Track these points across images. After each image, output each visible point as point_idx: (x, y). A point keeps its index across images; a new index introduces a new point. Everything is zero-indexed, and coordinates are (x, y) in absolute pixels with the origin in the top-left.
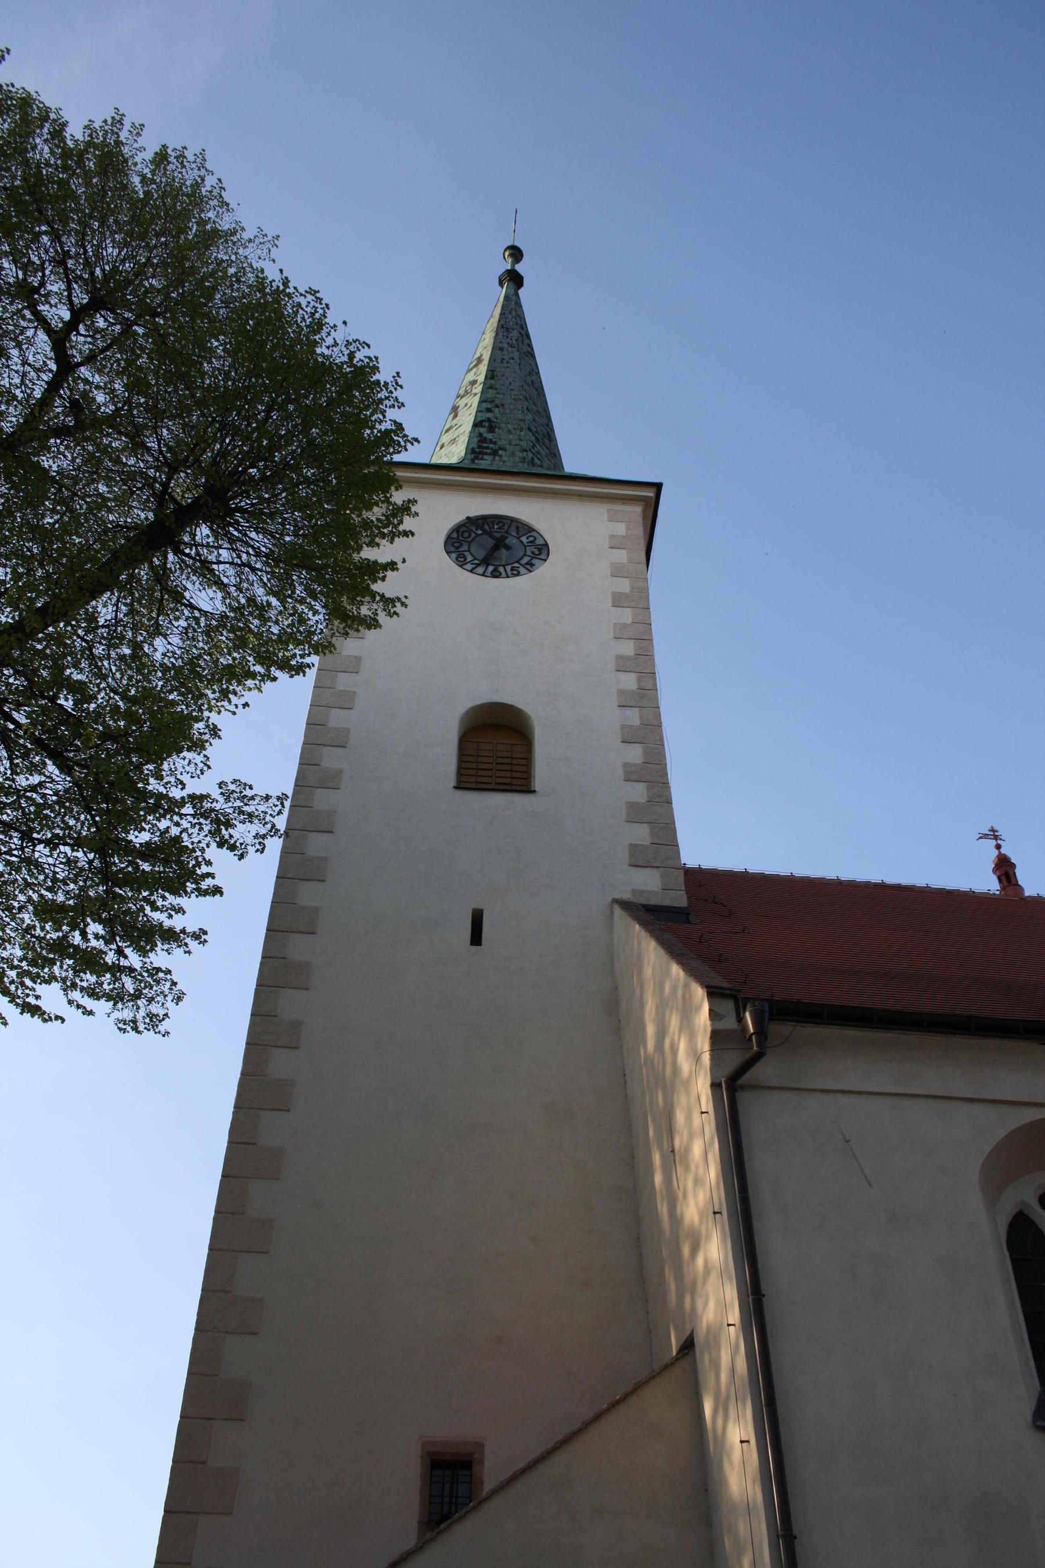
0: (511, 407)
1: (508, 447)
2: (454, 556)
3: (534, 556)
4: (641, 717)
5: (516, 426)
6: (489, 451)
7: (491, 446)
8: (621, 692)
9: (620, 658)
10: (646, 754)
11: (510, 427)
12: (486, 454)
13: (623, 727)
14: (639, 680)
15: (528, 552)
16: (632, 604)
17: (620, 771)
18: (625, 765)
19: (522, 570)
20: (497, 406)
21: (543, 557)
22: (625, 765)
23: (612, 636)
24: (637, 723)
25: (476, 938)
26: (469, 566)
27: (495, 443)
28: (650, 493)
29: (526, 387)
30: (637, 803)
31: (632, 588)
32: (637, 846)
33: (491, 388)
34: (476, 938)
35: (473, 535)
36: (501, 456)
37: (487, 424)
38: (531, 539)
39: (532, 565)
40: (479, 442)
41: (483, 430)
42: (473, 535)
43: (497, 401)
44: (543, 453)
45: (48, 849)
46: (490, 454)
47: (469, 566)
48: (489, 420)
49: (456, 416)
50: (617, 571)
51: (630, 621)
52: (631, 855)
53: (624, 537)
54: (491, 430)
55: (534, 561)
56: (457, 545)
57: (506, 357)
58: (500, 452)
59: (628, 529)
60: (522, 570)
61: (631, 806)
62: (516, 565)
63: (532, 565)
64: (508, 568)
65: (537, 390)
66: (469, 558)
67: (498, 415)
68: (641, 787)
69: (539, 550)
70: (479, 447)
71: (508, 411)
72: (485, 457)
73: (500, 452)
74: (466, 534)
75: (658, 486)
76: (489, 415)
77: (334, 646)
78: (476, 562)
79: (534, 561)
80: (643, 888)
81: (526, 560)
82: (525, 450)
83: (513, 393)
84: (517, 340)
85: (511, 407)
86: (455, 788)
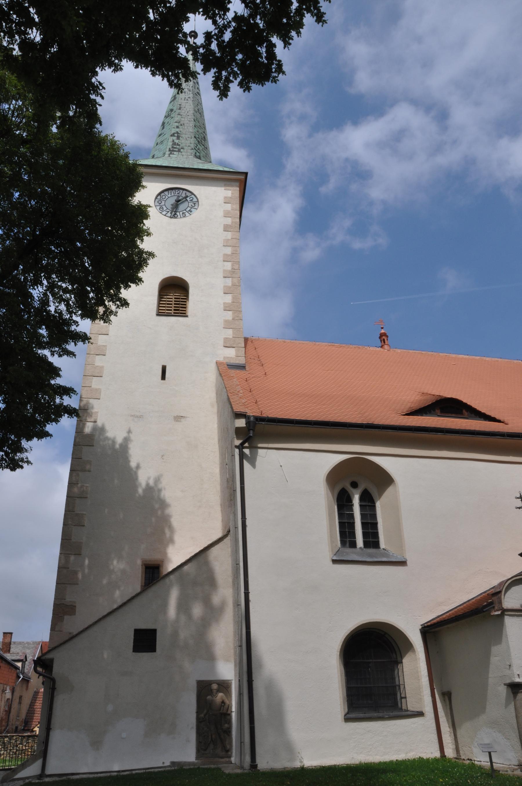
0: (188, 125)
1: (185, 147)
2: (158, 207)
3: (192, 207)
4: (232, 282)
5: (190, 136)
6: (176, 150)
7: (178, 147)
8: (224, 271)
9: (225, 255)
10: (233, 298)
11: (187, 136)
12: (175, 151)
13: (225, 286)
14: (232, 265)
15: (190, 206)
16: (232, 230)
17: (222, 306)
18: (224, 303)
19: (187, 214)
20: (181, 125)
21: (196, 207)
22: (224, 303)
23: (222, 245)
24: (230, 285)
25: (163, 377)
26: (164, 213)
27: (179, 145)
28: (243, 177)
29: (195, 113)
30: (228, 320)
31: (232, 222)
32: (227, 338)
33: (179, 114)
34: (163, 377)
35: (167, 197)
36: (181, 152)
37: (176, 135)
38: (191, 199)
39: (191, 211)
40: (173, 144)
41: (175, 138)
42: (167, 197)
43: (182, 123)
44: (201, 148)
45: (51, 141)
46: (177, 151)
47: (164, 213)
48: (177, 133)
49: (163, 128)
50: (227, 215)
51: (230, 238)
52: (225, 342)
53: (231, 198)
54: (178, 138)
55: (192, 210)
56: (160, 202)
57: (187, 97)
58: (182, 150)
59: (232, 194)
60: (187, 214)
61: (226, 321)
62: (185, 211)
63: (191, 211)
64: (181, 213)
65: (200, 114)
66: (165, 208)
67: (181, 130)
68: (230, 313)
69: (194, 204)
70: (173, 147)
71: (186, 127)
72: (175, 153)
73: (182, 150)
74: (164, 197)
75: (246, 174)
76: (178, 130)
77: (301, 33)
78: (168, 210)
79: (192, 210)
80: (228, 356)
81: (189, 209)
82: (192, 149)
83: (189, 117)
84: (192, 87)
85: (188, 125)
86: (157, 315)
